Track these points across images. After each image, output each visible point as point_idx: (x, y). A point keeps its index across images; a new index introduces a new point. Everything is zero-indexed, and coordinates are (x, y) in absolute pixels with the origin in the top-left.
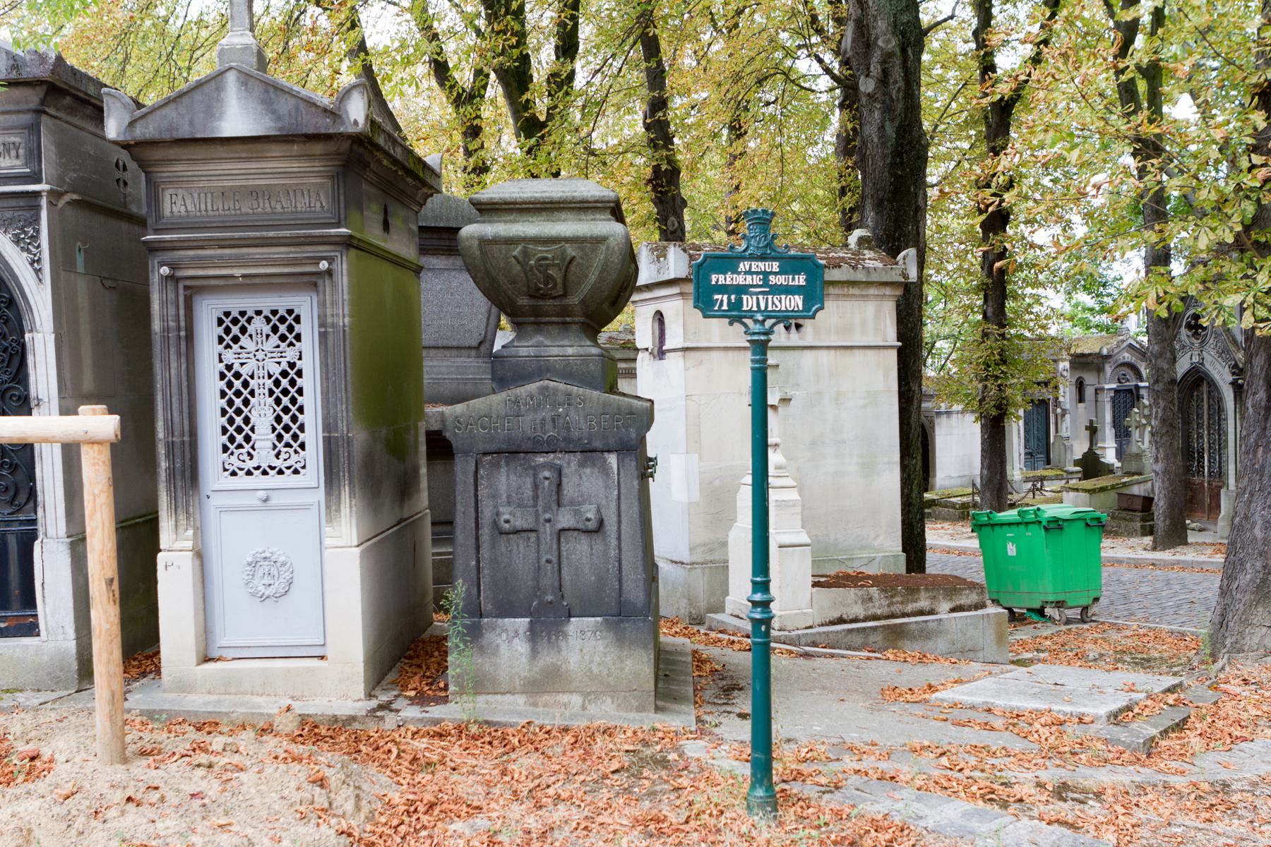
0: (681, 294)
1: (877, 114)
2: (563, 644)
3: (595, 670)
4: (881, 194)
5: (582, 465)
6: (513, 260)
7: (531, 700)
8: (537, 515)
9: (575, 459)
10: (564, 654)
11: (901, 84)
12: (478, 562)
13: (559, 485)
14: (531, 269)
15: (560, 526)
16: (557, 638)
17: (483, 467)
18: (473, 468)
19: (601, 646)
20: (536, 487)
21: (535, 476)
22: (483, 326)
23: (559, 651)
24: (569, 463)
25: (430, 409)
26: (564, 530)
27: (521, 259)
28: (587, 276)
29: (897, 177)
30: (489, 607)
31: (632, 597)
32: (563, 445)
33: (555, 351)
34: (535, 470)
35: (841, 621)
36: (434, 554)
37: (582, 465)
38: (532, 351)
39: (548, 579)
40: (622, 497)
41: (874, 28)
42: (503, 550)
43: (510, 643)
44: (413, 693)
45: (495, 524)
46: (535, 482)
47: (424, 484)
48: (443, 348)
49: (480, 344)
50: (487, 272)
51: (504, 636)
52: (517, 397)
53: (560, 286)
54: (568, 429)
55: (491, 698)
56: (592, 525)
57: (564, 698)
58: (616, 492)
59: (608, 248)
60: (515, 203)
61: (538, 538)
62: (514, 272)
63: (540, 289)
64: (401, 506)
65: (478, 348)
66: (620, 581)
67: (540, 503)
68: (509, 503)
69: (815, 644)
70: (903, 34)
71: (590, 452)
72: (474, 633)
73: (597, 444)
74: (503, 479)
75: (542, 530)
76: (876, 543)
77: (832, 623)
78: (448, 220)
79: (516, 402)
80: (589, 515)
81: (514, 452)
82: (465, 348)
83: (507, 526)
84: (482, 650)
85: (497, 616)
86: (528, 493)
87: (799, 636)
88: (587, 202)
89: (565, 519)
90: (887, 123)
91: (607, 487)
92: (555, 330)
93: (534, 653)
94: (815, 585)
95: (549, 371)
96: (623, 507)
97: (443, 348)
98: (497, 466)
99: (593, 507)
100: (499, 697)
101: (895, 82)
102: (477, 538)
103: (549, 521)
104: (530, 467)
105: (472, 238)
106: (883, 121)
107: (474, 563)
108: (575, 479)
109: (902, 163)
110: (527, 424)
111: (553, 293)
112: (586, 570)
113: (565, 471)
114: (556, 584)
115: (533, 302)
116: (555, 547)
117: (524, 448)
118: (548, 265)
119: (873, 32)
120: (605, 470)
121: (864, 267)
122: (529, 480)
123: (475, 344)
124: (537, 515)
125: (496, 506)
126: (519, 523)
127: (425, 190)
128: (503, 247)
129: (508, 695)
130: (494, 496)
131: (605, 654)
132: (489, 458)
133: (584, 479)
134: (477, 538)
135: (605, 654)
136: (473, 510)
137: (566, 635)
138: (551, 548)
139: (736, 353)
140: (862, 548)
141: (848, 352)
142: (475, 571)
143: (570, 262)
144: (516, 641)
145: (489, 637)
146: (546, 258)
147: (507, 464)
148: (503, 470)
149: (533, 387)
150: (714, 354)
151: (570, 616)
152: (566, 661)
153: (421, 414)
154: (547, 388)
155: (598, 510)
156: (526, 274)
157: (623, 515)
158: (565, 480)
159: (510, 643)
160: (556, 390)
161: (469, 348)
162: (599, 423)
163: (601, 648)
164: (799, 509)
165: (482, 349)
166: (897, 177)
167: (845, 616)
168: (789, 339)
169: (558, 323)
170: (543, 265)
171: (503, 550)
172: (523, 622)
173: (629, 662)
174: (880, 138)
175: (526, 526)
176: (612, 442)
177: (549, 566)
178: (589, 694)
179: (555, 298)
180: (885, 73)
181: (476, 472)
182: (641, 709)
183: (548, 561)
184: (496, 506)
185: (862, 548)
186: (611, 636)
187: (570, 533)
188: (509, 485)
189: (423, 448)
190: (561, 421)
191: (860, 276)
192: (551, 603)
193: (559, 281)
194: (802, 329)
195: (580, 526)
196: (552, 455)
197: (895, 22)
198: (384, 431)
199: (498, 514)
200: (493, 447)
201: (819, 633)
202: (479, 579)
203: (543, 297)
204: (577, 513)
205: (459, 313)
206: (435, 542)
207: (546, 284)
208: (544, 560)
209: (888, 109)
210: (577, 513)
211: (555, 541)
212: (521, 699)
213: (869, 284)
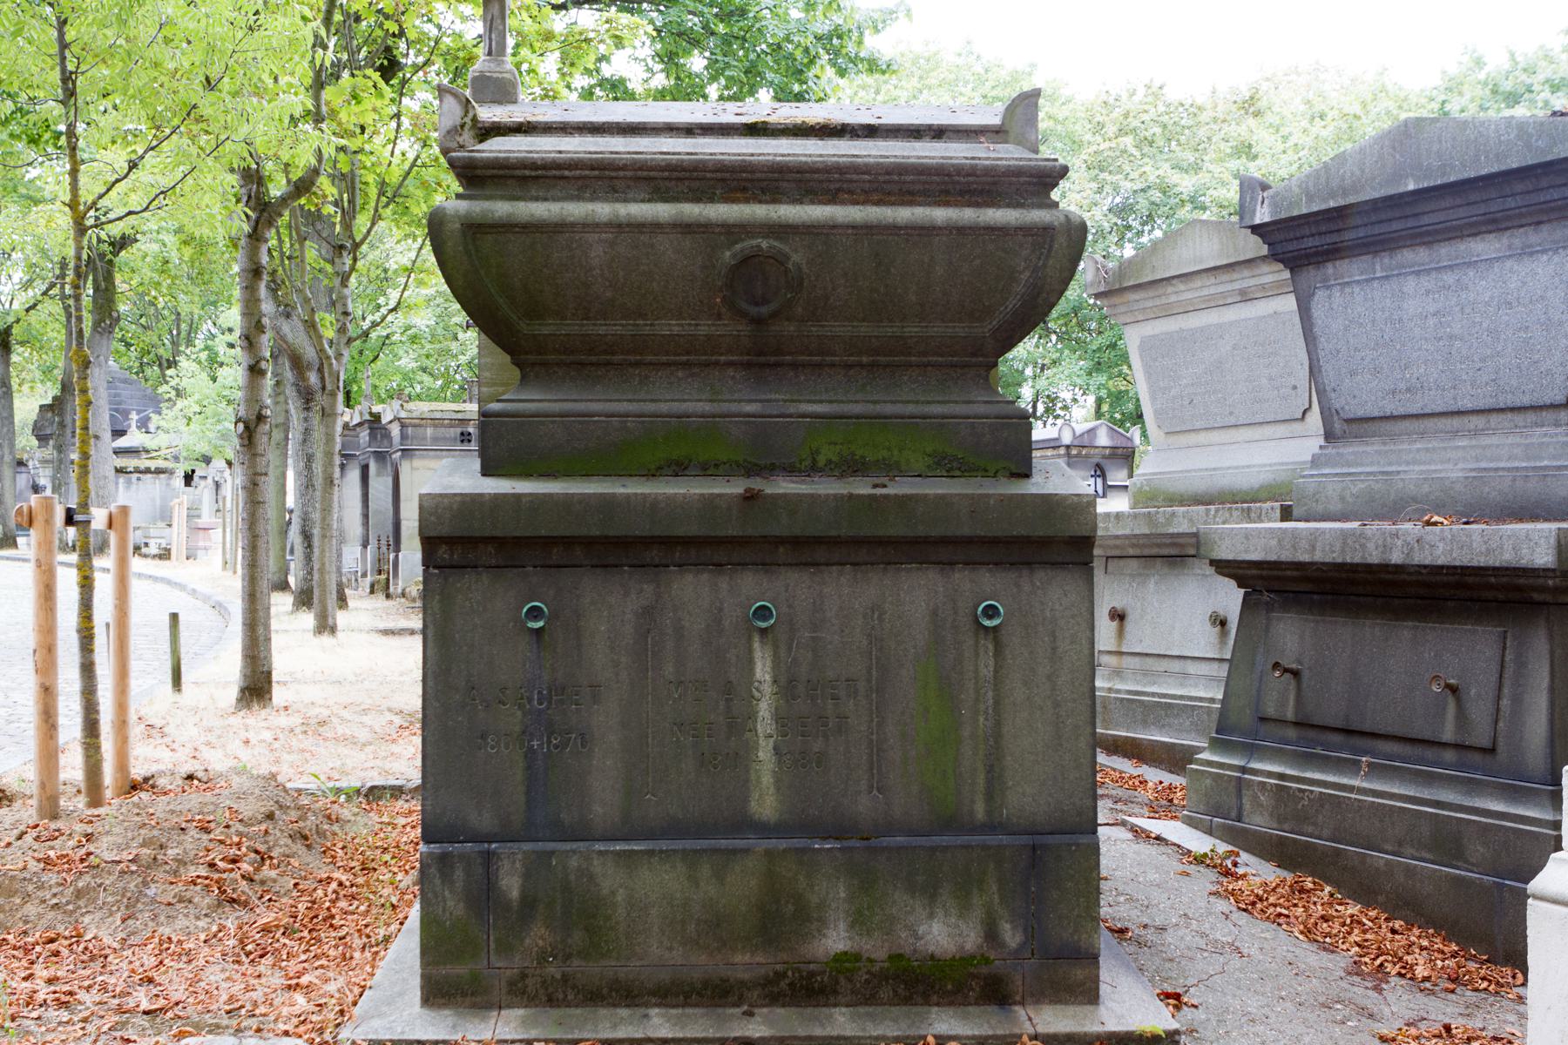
48: (1512, 409)
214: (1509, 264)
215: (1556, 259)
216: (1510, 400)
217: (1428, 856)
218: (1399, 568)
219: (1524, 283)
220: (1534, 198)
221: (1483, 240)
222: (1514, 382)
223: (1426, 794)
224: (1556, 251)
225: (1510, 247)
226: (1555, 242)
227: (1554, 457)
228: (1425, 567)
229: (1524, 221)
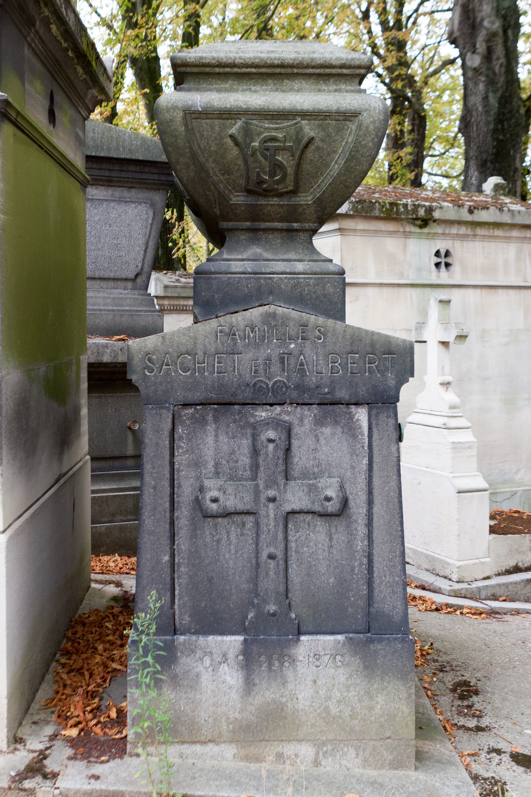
0: (340, 230)
1: (481, 86)
2: (289, 674)
3: (334, 710)
4: (485, 156)
5: (319, 422)
6: (229, 141)
7: (242, 752)
8: (257, 492)
9: (309, 414)
10: (290, 686)
11: (503, 60)
12: (173, 556)
13: (288, 450)
14: (253, 154)
15: (288, 508)
16: (282, 664)
17: (183, 423)
18: (170, 425)
19: (341, 675)
20: (255, 452)
21: (254, 437)
22: (140, 258)
23: (284, 683)
24: (301, 420)
25: (94, 341)
26: (294, 512)
27: (240, 139)
28: (327, 166)
29: (499, 142)
30: (187, 619)
31: (387, 608)
32: (294, 394)
33: (280, 266)
34: (255, 430)
35: (517, 569)
36: (93, 492)
37: (319, 422)
38: (249, 266)
39: (270, 582)
40: (375, 467)
41: (480, 11)
42: (208, 539)
43: (215, 668)
44: (74, 732)
45: (198, 503)
46: (254, 445)
47: (85, 427)
48: (100, 279)
49: (137, 276)
50: (194, 156)
51: (207, 661)
52: (232, 327)
53: (290, 179)
54: (302, 372)
55: (186, 749)
56: (332, 507)
57: (289, 749)
58: (365, 461)
59: (360, 126)
60: (233, 65)
61: (257, 524)
62: (230, 157)
63: (262, 182)
64: (60, 460)
65: (134, 280)
66: (370, 583)
67: (262, 475)
68: (217, 474)
69: (495, 598)
70: (504, 17)
71: (330, 404)
72: (168, 658)
73: (342, 394)
74: (210, 440)
75: (263, 512)
76: (517, 477)
77: (509, 572)
78: (109, 150)
79: (231, 334)
80: (330, 493)
81: (225, 403)
82: (122, 279)
83: (214, 506)
84: (175, 680)
85: (197, 633)
86: (245, 460)
87: (479, 589)
88: (331, 66)
89: (296, 498)
90: (491, 95)
91: (353, 453)
92: (276, 239)
93: (249, 684)
94: (493, 530)
95: (271, 293)
96: (377, 482)
97: (100, 279)
98: (201, 422)
99: (335, 481)
100: (198, 748)
101: (498, 59)
102: (172, 523)
103: (273, 500)
104: (248, 424)
105: (175, 108)
106: (487, 92)
107: (167, 558)
108: (310, 442)
109: (503, 129)
110: (246, 364)
111: (281, 188)
112: (323, 569)
113: (296, 430)
114: (282, 588)
115: (251, 200)
116: (280, 536)
117: (240, 398)
118: (277, 149)
119: (479, 16)
120: (351, 429)
121: (509, 210)
122: (246, 443)
123: (132, 275)
124: (257, 492)
125: (198, 478)
126: (231, 502)
127: (95, 92)
128: (217, 122)
129: (211, 745)
130: (197, 464)
131: (348, 688)
132: (191, 411)
133: (322, 441)
134: (172, 523)
135: (348, 688)
136: (167, 484)
137: (293, 661)
138: (275, 537)
139: (390, 289)
140: (505, 482)
141: (492, 291)
142: (168, 570)
143: (307, 146)
144: (224, 668)
145: (185, 662)
146: (274, 139)
147: (216, 420)
148: (211, 428)
149: (255, 314)
150: (370, 291)
151: (300, 633)
152: (294, 697)
153: (83, 347)
154: (274, 315)
155: (342, 487)
156: (245, 160)
157: (376, 492)
158: (295, 443)
159: (215, 668)
160: (286, 319)
161: (126, 279)
162: (344, 366)
163: (343, 679)
164: (474, 452)
165: (139, 280)
166: (499, 142)
167: (520, 564)
168: (439, 277)
169: (281, 230)
170: (270, 148)
171: (208, 539)
172: (235, 641)
173: (380, 699)
174: (484, 107)
175: (240, 507)
176: (362, 392)
177: (272, 564)
178: (324, 744)
179: (281, 195)
180: (490, 51)
181: (173, 431)
182: (396, 765)
183: (271, 557)
184: (198, 478)
185: (505, 482)
186: (356, 661)
187: (301, 517)
188: (217, 449)
189: (84, 386)
190: (292, 361)
191: (506, 218)
192: (274, 615)
193: (290, 171)
194: (451, 268)
195: (317, 508)
196: (278, 409)
197: (498, 6)
198: (43, 369)
199: (202, 489)
200: (198, 396)
201: (499, 585)
202: (173, 579)
203: (267, 193)
204: (312, 489)
205: (117, 245)
206: (95, 478)
207: (272, 175)
208: (264, 555)
209: (491, 82)
210: (312, 489)
211: (281, 528)
212: (229, 751)
213: (513, 226)
214: (112, 204)
215: (139, 207)
216: (102, 274)
217: (131, 518)
218: (106, 365)
219: (120, 216)
220: (139, 176)
221: (97, 188)
222: (106, 265)
223: (123, 485)
224: (140, 203)
225: (112, 195)
226: (137, 198)
227: (130, 305)
228: (119, 363)
229: (126, 185)
